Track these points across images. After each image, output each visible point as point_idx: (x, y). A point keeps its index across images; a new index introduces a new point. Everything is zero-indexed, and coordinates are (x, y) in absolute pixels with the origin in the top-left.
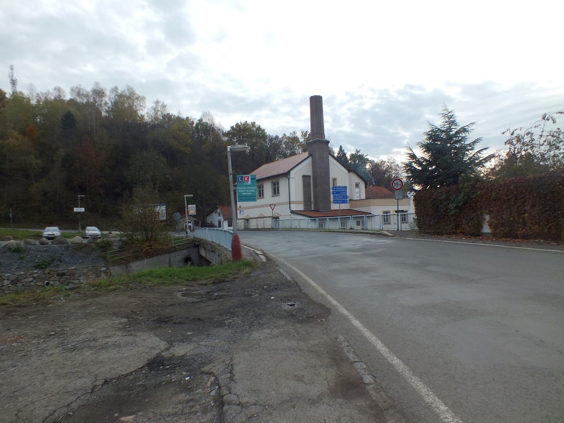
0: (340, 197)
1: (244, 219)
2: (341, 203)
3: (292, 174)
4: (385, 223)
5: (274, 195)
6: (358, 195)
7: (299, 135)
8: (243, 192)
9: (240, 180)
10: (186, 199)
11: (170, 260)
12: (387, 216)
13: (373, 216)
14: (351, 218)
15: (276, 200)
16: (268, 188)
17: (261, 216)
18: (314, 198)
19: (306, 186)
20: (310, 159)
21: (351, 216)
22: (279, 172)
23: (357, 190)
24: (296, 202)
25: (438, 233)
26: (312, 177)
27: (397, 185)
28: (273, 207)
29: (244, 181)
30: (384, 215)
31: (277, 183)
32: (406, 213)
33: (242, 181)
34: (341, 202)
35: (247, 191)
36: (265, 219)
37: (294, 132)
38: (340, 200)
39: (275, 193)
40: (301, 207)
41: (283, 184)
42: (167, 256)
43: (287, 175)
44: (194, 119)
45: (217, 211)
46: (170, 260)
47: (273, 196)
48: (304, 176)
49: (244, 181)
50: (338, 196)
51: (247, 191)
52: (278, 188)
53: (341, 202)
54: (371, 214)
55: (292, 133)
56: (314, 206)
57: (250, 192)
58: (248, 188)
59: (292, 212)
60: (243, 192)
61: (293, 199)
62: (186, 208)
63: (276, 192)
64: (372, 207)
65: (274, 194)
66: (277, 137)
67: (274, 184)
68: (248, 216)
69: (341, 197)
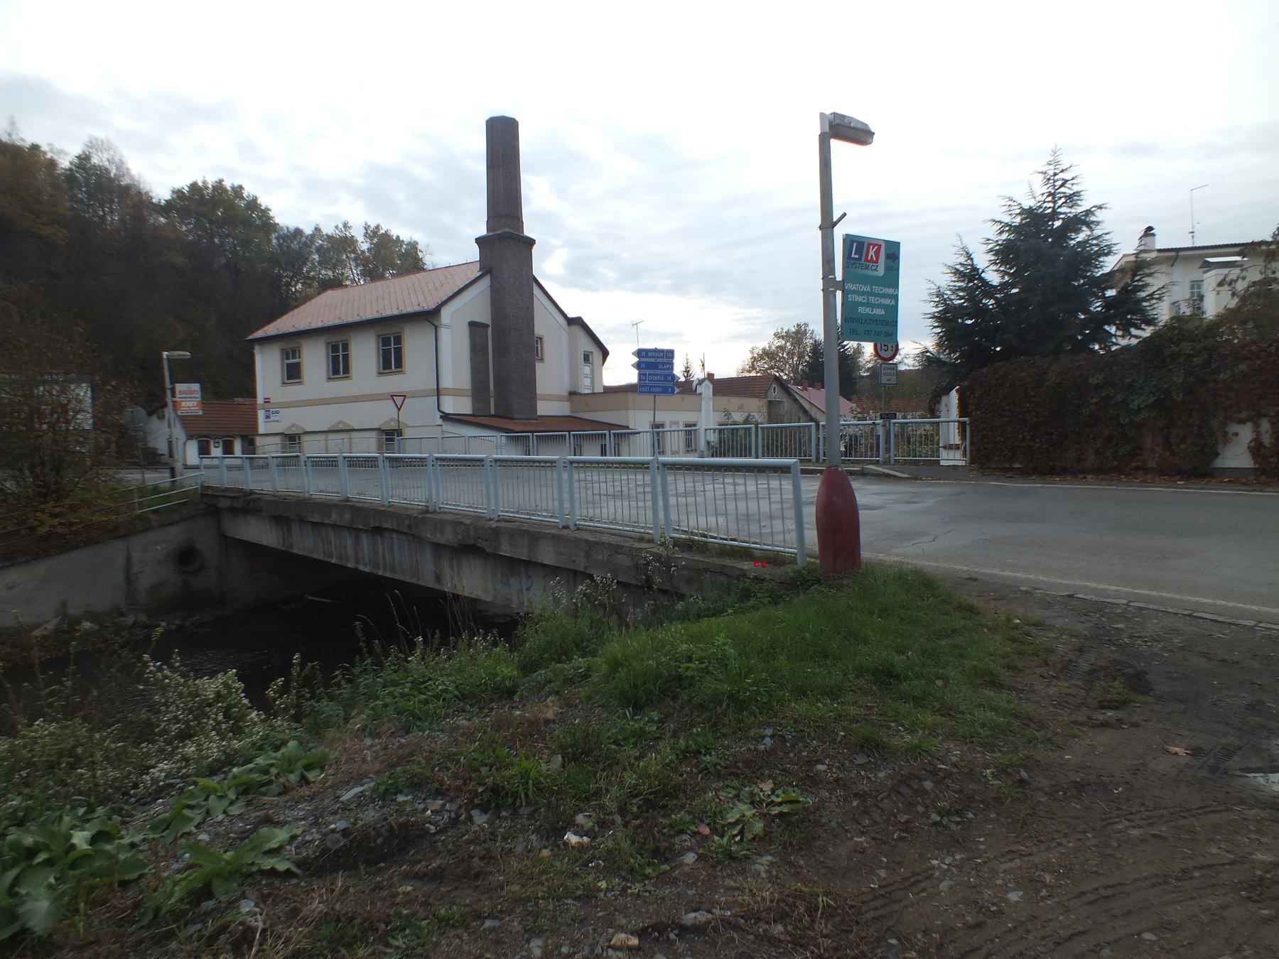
0: (655, 378)
1: (378, 429)
2: (658, 393)
3: (446, 315)
4: (690, 449)
5: (385, 371)
6: (587, 382)
7: (358, 233)
8: (862, 304)
9: (853, 256)
10: (169, 366)
11: (129, 560)
12: (658, 433)
13: (631, 433)
14: (607, 436)
15: (393, 383)
16: (364, 352)
17: (341, 427)
18: (497, 383)
19: (477, 350)
20: (486, 282)
21: (569, 432)
22: (361, 315)
23: (587, 370)
24: (455, 392)
25: (1006, 472)
26: (490, 330)
27: (886, 348)
28: (399, 400)
29: (866, 260)
30: (720, 430)
31: (395, 338)
32: (660, 430)
33: (859, 259)
34: (658, 389)
35: (873, 300)
36: (354, 435)
37: (345, 225)
38: (656, 387)
39: (336, 371)
40: (463, 406)
41: (415, 344)
42: (119, 545)
43: (429, 317)
44: (60, 152)
45: (163, 412)
46: (129, 560)
47: (329, 379)
48: (472, 325)
49: (866, 260)
50: (652, 375)
51: (873, 300)
52: (346, 358)
53: (658, 389)
54: (627, 428)
55: (341, 226)
56: (495, 403)
57: (879, 306)
58: (876, 289)
59: (446, 417)
60: (862, 304)
61: (447, 383)
62: (169, 393)
63: (391, 360)
64: (631, 412)
65: (334, 374)
66: (298, 232)
67: (335, 348)
68: (293, 425)
69: (658, 378)
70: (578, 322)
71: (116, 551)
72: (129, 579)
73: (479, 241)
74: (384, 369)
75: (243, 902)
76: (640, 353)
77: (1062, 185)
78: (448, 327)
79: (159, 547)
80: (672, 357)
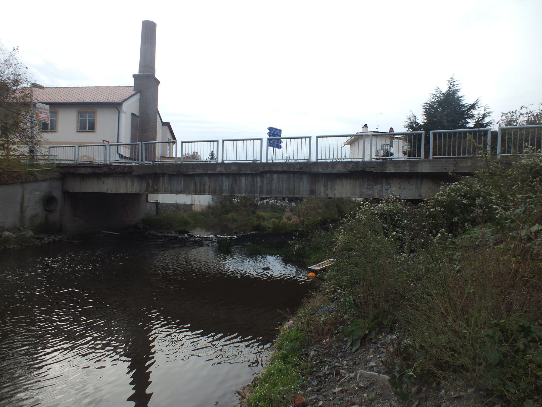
6: (168, 153)
19: (134, 127)
20: (137, 97)
70: (167, 125)
71: (15, 191)
72: (22, 211)
73: (134, 76)
74: (80, 130)
75: (425, 390)
76: (271, 129)
77: (453, 87)
78: (125, 113)
79: (37, 193)
80: (281, 133)
